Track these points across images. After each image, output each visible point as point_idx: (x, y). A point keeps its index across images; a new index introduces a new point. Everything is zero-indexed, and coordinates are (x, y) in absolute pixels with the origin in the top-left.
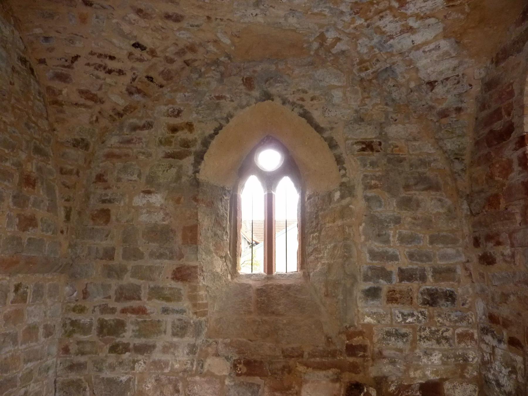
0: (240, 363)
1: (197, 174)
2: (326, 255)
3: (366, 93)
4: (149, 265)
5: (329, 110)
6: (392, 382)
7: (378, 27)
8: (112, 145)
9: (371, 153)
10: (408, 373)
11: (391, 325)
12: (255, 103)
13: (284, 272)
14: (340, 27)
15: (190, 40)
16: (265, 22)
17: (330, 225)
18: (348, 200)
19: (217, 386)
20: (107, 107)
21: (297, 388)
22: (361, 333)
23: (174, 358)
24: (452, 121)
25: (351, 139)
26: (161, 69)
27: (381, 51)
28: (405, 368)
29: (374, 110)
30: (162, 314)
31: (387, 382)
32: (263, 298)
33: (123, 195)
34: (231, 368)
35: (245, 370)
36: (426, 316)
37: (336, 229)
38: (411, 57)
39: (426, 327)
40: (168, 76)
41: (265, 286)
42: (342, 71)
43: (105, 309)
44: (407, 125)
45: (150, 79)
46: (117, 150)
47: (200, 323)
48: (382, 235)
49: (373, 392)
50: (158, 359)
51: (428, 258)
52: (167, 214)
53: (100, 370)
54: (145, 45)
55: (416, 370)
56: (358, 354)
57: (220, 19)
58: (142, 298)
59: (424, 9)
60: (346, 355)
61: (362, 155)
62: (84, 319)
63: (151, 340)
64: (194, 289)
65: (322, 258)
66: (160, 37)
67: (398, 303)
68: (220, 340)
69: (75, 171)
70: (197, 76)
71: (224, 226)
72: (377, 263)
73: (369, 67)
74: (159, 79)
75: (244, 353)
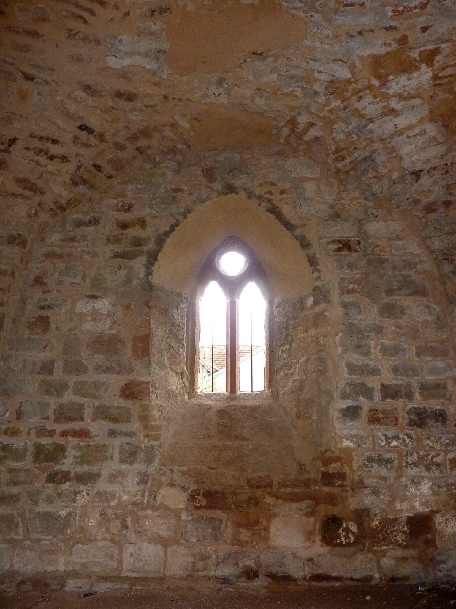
0: (198, 494)
1: (150, 276)
2: (297, 370)
3: (343, 186)
4: (93, 380)
5: (300, 205)
6: (376, 515)
7: (356, 110)
8: (52, 243)
9: (348, 253)
10: (394, 504)
11: (373, 449)
12: (217, 197)
13: (249, 391)
14: (313, 110)
15: (144, 124)
16: (229, 104)
17: (303, 335)
18: (322, 306)
19: (172, 521)
20: (48, 199)
21: (265, 523)
22: (338, 459)
23: (121, 488)
24: (440, 217)
25: (326, 237)
26: (111, 156)
27: (360, 137)
28: (390, 499)
29: (351, 205)
30: (108, 437)
31: (369, 516)
32: (225, 421)
33: (65, 300)
34: (188, 499)
35: (204, 502)
36: (414, 438)
37: (309, 339)
38: (394, 143)
39: (413, 452)
40: (117, 165)
41: (227, 407)
42: (315, 162)
43: (42, 432)
44: (390, 222)
45: (98, 168)
46: (59, 249)
47: (153, 448)
48: (362, 346)
49: (353, 527)
50: (103, 490)
51: (415, 372)
52: (115, 322)
53: (36, 503)
54: (93, 128)
55: (403, 500)
56: (336, 483)
57: (179, 99)
58: (86, 419)
59: (407, 88)
60: (322, 485)
61: (338, 255)
62: (17, 443)
63: (96, 468)
64: (146, 408)
65: (293, 374)
66: (109, 119)
67: (381, 424)
68: (176, 468)
69: (9, 272)
70: (151, 166)
71: (180, 337)
72: (356, 379)
73: (346, 156)
74: (108, 169)
75: (204, 483)
